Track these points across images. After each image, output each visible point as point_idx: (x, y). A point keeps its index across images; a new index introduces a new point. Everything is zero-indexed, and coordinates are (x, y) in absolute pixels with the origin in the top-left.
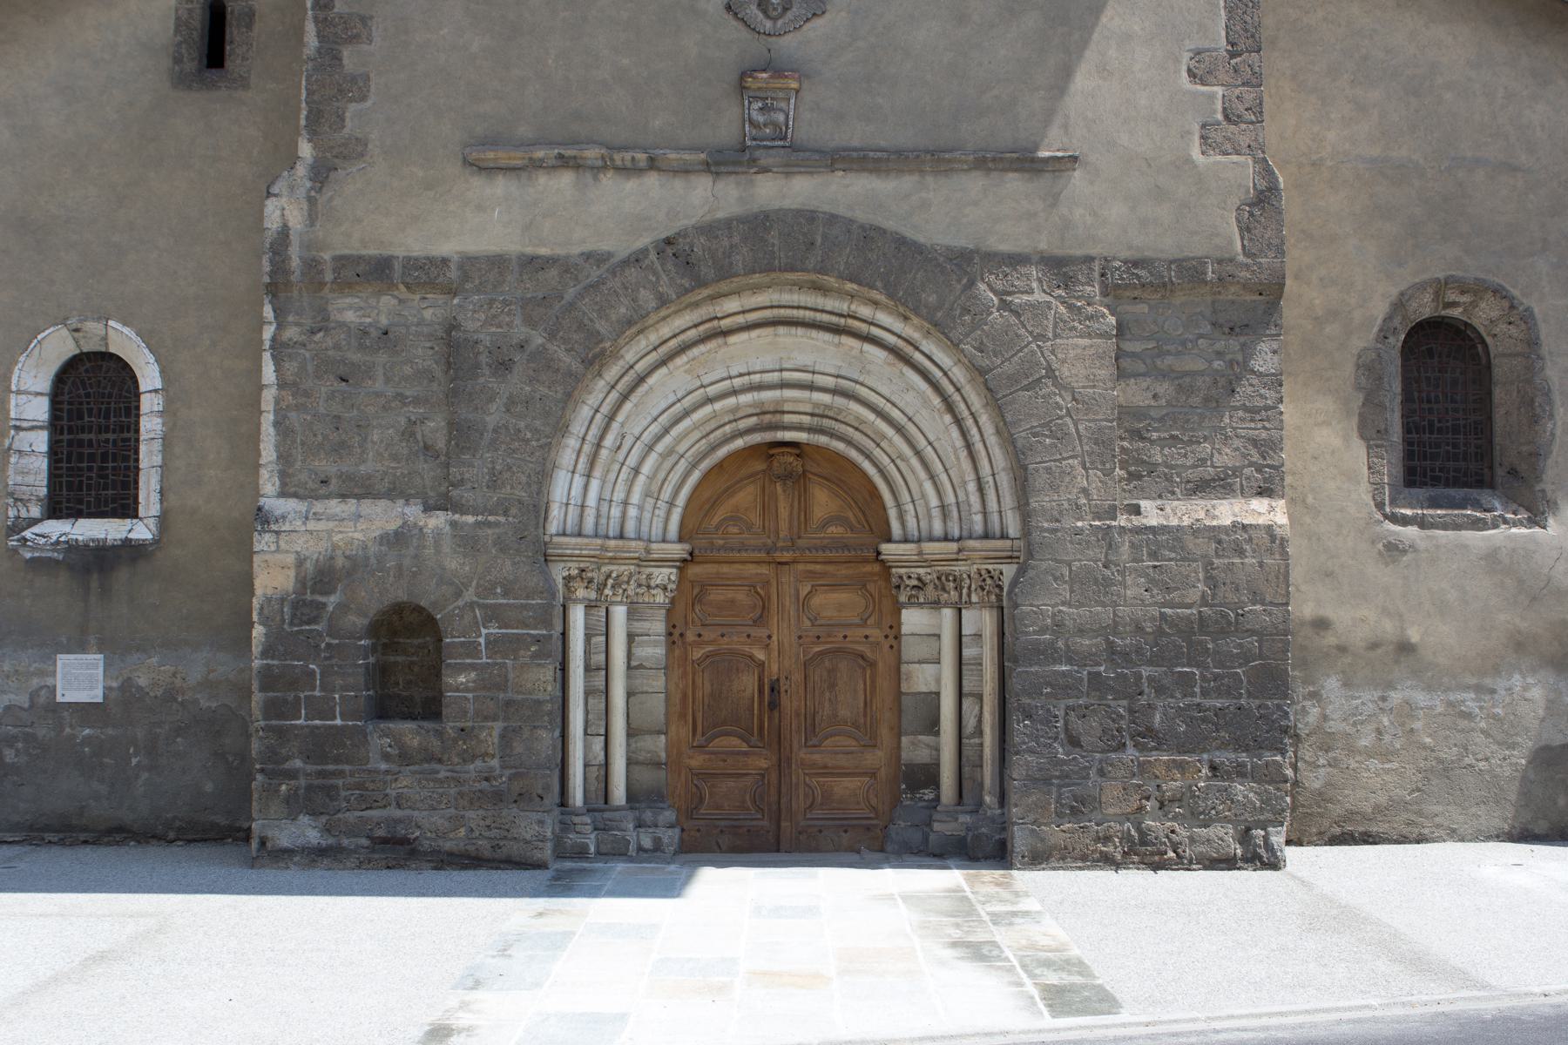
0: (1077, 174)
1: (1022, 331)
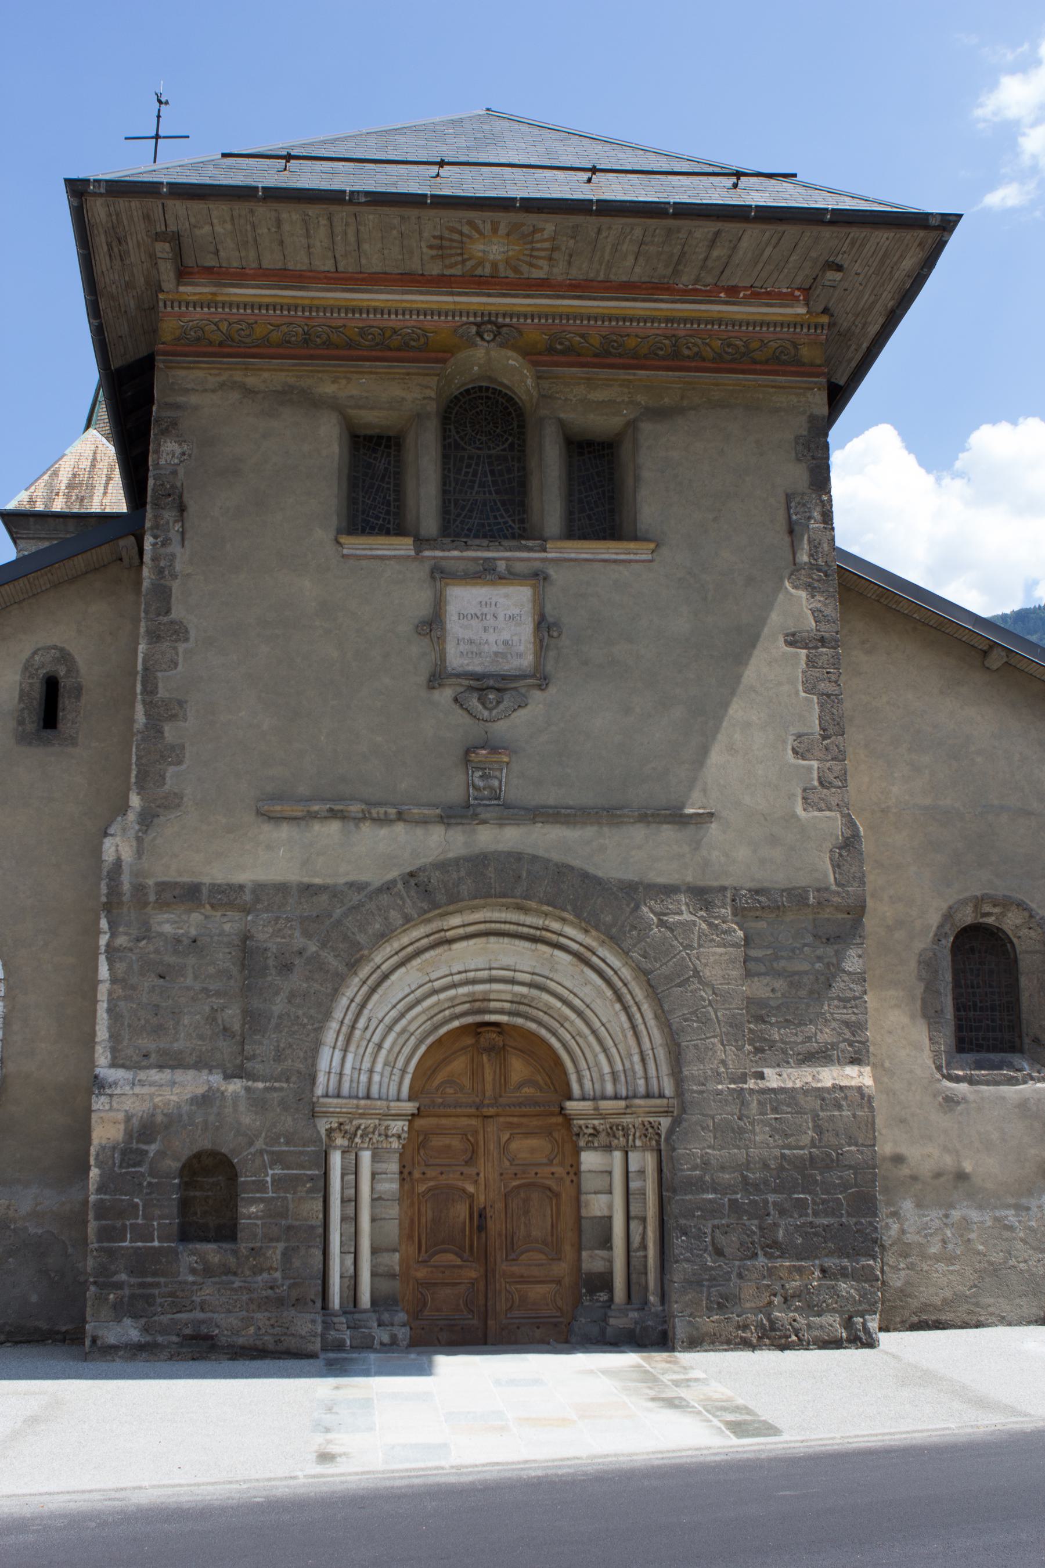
0: (713, 826)
1: (675, 943)
